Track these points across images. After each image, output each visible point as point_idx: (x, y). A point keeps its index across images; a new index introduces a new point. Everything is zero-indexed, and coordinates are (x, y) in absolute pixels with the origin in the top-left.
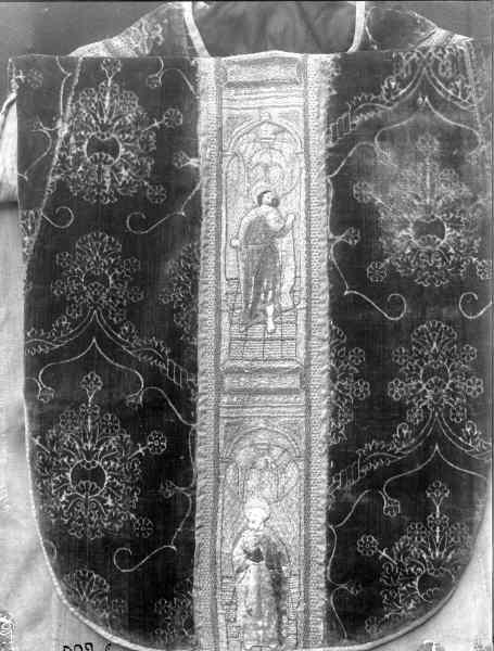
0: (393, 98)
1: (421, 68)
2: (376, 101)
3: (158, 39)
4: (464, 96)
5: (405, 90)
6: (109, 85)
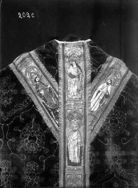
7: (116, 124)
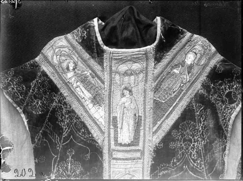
0: (175, 166)
1: (186, 155)
2: (168, 167)
3: (85, 36)
4: (200, 166)
5: (179, 163)
6: (70, 159)
7: (74, 115)
